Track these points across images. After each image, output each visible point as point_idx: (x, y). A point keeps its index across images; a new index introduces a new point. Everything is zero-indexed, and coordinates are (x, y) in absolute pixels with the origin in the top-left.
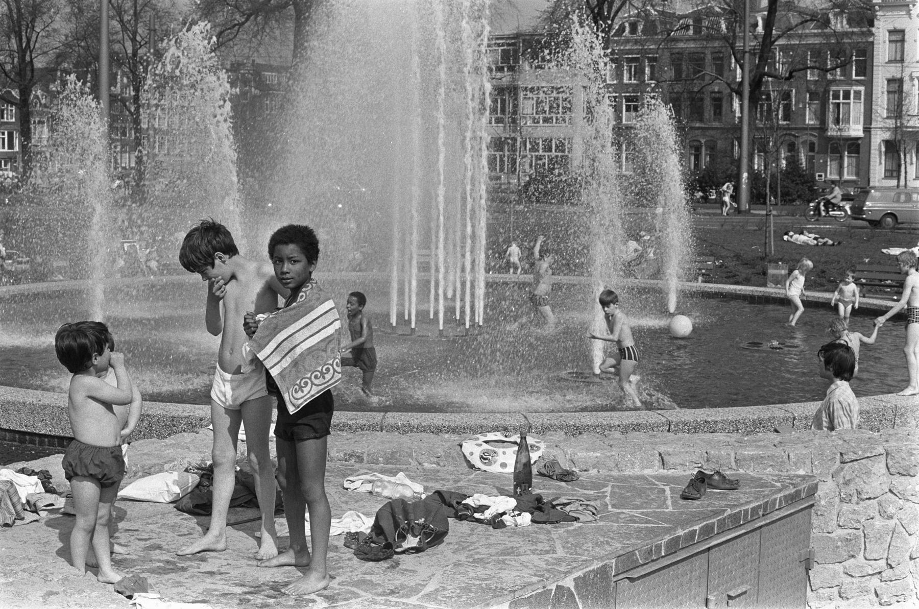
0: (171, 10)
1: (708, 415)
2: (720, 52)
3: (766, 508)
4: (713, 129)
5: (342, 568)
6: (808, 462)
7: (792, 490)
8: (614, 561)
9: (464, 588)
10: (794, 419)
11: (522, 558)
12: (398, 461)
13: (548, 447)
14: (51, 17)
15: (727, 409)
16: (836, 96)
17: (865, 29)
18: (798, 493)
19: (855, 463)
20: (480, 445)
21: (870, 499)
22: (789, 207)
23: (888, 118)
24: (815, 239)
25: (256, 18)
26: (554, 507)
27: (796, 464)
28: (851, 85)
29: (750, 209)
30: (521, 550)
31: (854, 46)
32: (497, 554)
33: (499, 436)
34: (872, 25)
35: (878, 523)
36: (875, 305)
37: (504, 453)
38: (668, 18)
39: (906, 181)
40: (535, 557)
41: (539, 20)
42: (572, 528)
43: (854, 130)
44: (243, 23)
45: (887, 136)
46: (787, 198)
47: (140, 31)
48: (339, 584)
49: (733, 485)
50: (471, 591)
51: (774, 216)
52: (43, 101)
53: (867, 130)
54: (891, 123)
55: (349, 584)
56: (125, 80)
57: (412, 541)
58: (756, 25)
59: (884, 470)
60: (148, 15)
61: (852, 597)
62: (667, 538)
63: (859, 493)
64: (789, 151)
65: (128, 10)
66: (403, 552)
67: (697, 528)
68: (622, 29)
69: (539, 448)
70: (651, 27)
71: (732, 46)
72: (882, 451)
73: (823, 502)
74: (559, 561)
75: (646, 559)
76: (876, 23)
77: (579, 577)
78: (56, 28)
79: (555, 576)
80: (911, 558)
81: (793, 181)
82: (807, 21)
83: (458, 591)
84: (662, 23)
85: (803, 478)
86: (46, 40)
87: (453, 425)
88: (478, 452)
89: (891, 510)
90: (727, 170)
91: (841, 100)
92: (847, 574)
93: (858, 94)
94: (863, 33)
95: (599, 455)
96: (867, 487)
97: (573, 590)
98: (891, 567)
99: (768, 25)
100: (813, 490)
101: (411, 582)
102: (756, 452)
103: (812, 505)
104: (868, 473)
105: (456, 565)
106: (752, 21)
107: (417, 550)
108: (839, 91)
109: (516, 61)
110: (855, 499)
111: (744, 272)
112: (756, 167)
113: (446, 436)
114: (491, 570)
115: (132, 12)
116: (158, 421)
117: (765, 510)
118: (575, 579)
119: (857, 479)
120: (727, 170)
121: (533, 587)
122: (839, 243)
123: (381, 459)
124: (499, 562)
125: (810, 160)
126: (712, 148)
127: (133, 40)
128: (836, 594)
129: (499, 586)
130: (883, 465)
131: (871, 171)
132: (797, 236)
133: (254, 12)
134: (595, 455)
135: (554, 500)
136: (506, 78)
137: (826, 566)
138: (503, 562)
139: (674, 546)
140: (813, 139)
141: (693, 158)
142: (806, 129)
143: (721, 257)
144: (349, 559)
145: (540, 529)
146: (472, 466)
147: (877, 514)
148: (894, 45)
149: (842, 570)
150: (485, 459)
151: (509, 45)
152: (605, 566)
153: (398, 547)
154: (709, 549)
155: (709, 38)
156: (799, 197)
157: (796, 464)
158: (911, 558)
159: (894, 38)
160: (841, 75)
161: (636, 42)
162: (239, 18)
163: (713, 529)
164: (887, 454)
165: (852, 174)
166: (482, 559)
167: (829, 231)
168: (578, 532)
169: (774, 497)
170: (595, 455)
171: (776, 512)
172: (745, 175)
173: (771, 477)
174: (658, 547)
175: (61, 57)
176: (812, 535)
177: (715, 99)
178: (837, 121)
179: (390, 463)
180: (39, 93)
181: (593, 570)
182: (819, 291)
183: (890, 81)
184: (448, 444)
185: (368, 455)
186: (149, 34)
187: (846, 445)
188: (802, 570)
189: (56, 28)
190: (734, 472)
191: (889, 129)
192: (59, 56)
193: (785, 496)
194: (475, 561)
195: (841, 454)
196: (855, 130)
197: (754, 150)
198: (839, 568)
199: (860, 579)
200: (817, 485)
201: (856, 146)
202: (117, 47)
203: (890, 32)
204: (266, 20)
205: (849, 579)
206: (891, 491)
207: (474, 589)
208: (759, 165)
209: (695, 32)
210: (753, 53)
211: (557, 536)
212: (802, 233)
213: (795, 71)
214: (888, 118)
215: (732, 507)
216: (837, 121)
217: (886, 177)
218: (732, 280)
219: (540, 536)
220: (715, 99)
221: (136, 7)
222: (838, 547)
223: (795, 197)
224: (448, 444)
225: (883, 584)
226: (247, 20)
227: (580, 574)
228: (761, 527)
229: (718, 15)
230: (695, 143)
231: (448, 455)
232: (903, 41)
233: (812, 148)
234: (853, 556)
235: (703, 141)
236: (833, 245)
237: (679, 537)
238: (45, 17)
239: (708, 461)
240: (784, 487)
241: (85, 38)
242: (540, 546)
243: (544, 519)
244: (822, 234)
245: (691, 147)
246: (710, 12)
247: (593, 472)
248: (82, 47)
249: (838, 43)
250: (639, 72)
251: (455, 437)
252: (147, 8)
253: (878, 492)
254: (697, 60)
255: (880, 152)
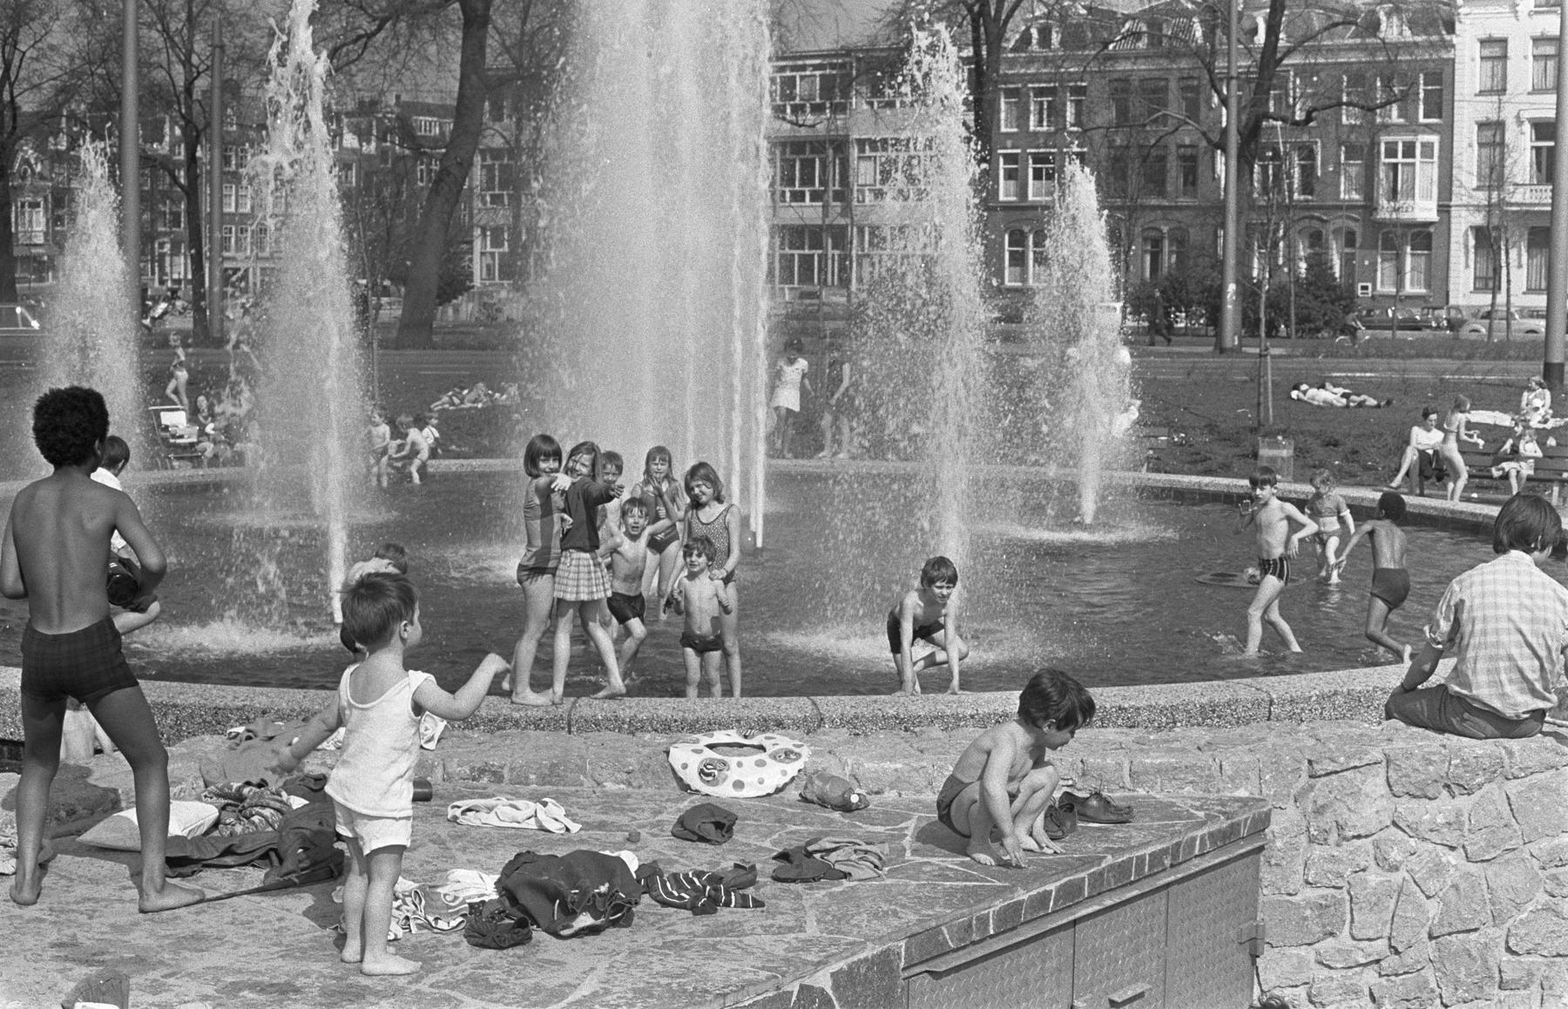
0: (253, 12)
1: (1124, 698)
2: (1192, 78)
3: (1178, 854)
4: (1179, 208)
5: (441, 958)
6: (1253, 776)
7: (1223, 823)
8: (903, 943)
9: (642, 991)
10: (1271, 702)
11: (746, 940)
12: (561, 780)
13: (815, 753)
14: (45, 25)
15: (1158, 687)
16: (1392, 152)
17: (1435, 38)
18: (1234, 828)
19: (1334, 777)
20: (700, 752)
21: (1359, 837)
22: (1308, 342)
23: (1478, 188)
24: (1344, 396)
25: (394, 25)
26: (809, 855)
27: (1232, 779)
28: (1415, 133)
29: (1241, 345)
30: (747, 926)
31: (1422, 66)
32: (705, 934)
33: (733, 736)
34: (1451, 29)
35: (1374, 878)
36: (1435, 508)
37: (740, 764)
38: (1105, 19)
39: (1508, 296)
40: (767, 938)
41: (879, 26)
42: (839, 889)
43: (1422, 210)
44: (374, 34)
45: (1479, 219)
46: (1307, 326)
47: (196, 47)
48: (431, 986)
49: (1121, 815)
50: (651, 996)
51: (1273, 357)
52: (38, 168)
53: (1444, 209)
54: (1481, 197)
55: (448, 985)
56: (178, 131)
57: (585, 920)
58: (1255, 31)
59: (1384, 790)
60: (212, 18)
61: (1332, 1003)
62: (999, 904)
63: (1340, 827)
64: (1312, 246)
65: (177, 14)
66: (577, 934)
67: (1052, 887)
68: (1025, 39)
69: (799, 756)
70: (1074, 37)
71: (1210, 69)
72: (1380, 757)
73: (1279, 844)
74: (807, 944)
75: (961, 940)
76: (1458, 26)
77: (841, 971)
78: (54, 45)
79: (797, 969)
80: (1431, 937)
81: (1316, 297)
82: (1336, 25)
83: (630, 995)
84: (1093, 29)
85: (1244, 802)
86: (37, 65)
87: (690, 717)
88: (695, 762)
89: (1395, 855)
90: (1205, 278)
91: (1400, 159)
92: (1321, 963)
93: (1427, 147)
94: (1432, 45)
95: (899, 766)
96: (1354, 817)
97: (830, 993)
98: (1397, 952)
99: (1272, 31)
100: (1262, 822)
101: (552, 980)
102: (1165, 760)
103: (1261, 848)
104: (1356, 794)
105: (633, 953)
106: (1246, 24)
107: (593, 930)
108: (1396, 143)
109: (846, 94)
110: (1333, 837)
111: (1221, 453)
112: (1255, 274)
113: (647, 736)
114: (691, 959)
115: (183, 15)
116: (191, 716)
117: (1175, 857)
118: (832, 974)
119: (1338, 804)
120: (1205, 278)
121: (759, 988)
122: (1389, 403)
123: (532, 777)
124: (705, 946)
125: (1347, 261)
126: (1180, 241)
127: (187, 63)
128: (1304, 996)
129: (700, 986)
130: (1381, 780)
131: (1452, 280)
132: (1313, 392)
133: (393, 15)
134: (893, 766)
135: (809, 843)
136: (818, 125)
137: (1288, 951)
138: (714, 946)
139: (1010, 918)
140: (1352, 224)
141: (1148, 258)
142: (1339, 208)
143: (1183, 429)
144: (456, 945)
145: (785, 891)
146: (686, 788)
147: (1373, 863)
148: (1489, 64)
149: (1312, 957)
150: (708, 775)
151: (833, 66)
152: (886, 953)
153: (565, 928)
154: (1075, 922)
155: (1172, 55)
156: (1326, 324)
157: (1232, 779)
158: (1431, 937)
159: (1487, 53)
160: (1400, 116)
161: (1046, 61)
162: (366, 25)
163: (1081, 889)
164: (1388, 762)
165: (1419, 284)
166: (677, 943)
167: (1369, 381)
168: (849, 896)
169: (1190, 835)
170: (893, 766)
171: (1196, 861)
172: (1232, 287)
173: (1190, 802)
174: (983, 921)
175: (66, 92)
176: (1261, 899)
177: (1183, 158)
178: (1394, 195)
179: (550, 783)
180: (30, 153)
181: (866, 960)
182: (1347, 485)
183: (1482, 126)
184: (647, 751)
185: (512, 769)
186: (212, 54)
187: (1319, 747)
188: (1244, 957)
189: (54, 45)
190: (1127, 794)
191: (1478, 208)
192: (61, 91)
193: (1211, 834)
194: (665, 945)
195: (1310, 762)
196: (1424, 209)
197: (1249, 246)
198: (1308, 953)
199: (1344, 972)
200: (1268, 815)
201: (1424, 237)
202: (159, 75)
203: (1483, 42)
204: (413, 28)
205: (1326, 972)
206: (1394, 824)
207: (657, 991)
208: (1262, 270)
209: (1151, 44)
210: (1243, 80)
211: (811, 902)
212: (1323, 387)
213: (1315, 109)
214: (1478, 188)
215: (1114, 852)
216: (1394, 195)
217: (1476, 290)
218: (1199, 467)
219: (783, 904)
220: (1183, 158)
221: (190, 9)
222: (1305, 919)
223: (1320, 323)
224: (647, 751)
225: (1383, 980)
226: (380, 29)
227: (842, 965)
228: (1168, 885)
229: (1188, 15)
230: (1153, 234)
231: (645, 769)
232: (1504, 57)
233: (1350, 240)
234: (1332, 934)
235: (1165, 229)
236: (1378, 406)
237: (1020, 903)
238: (35, 25)
239: (1084, 775)
240: (1210, 818)
241: (104, 61)
242: (779, 920)
243: (791, 875)
244: (1357, 387)
245: (1145, 240)
246: (1174, 10)
247: (890, 795)
248: (100, 76)
249: (1390, 61)
250: (1056, 112)
251: (661, 739)
252: (209, 9)
253: (1372, 828)
254: (1155, 92)
255: (1466, 246)
